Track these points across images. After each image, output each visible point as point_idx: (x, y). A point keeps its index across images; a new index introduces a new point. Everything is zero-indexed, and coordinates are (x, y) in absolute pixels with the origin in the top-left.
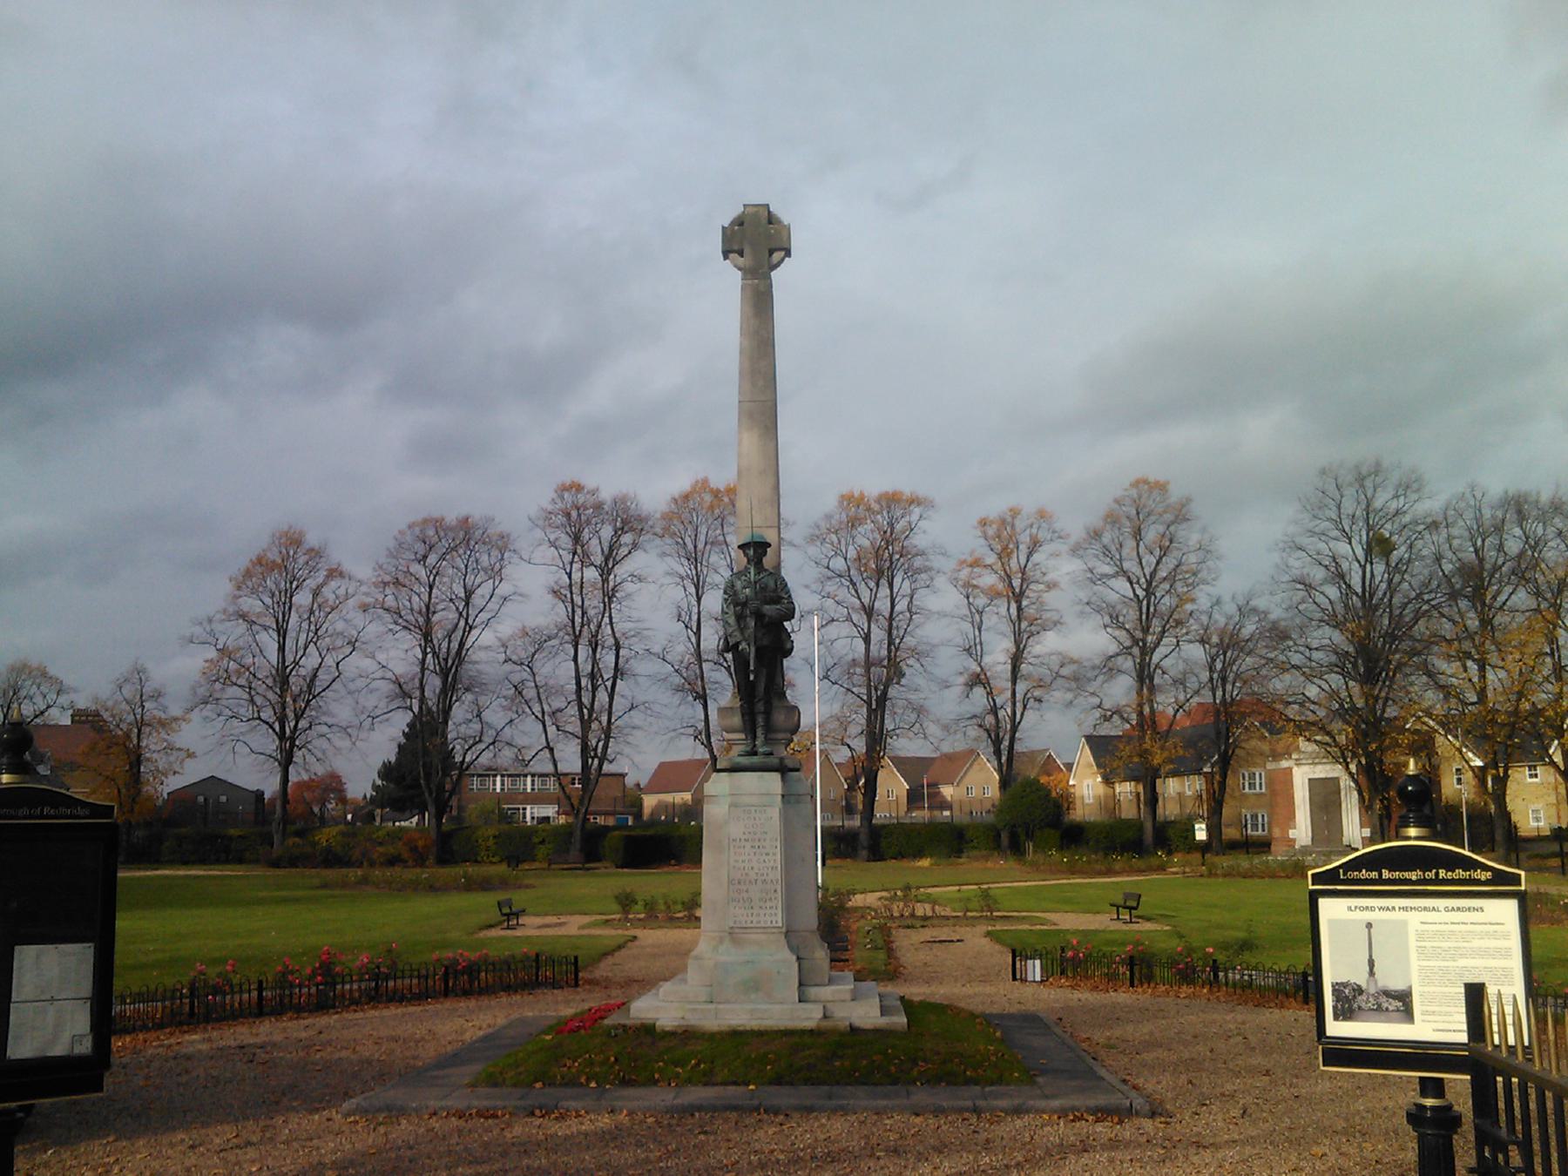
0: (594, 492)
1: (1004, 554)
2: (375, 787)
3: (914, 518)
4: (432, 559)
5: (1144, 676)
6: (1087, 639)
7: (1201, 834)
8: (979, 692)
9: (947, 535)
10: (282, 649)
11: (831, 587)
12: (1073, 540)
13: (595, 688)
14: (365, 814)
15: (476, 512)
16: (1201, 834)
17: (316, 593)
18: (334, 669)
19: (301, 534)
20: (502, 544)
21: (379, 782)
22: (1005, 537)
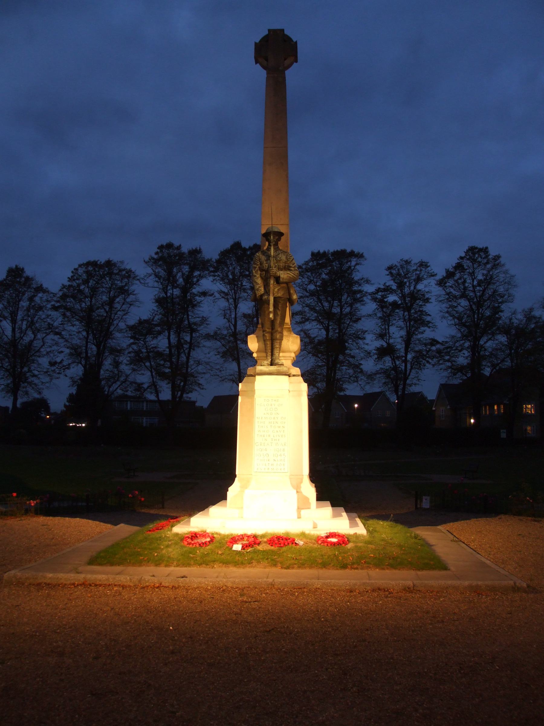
0: (179, 248)
1: (401, 285)
2: (65, 406)
3: (353, 263)
4: (91, 283)
5: (475, 349)
6: (442, 328)
7: (503, 435)
8: (388, 359)
9: (372, 275)
10: (14, 330)
11: (309, 301)
12: (439, 277)
13: (179, 354)
14: (62, 419)
15: (115, 258)
16: (503, 435)
17: (31, 299)
18: (41, 341)
19: (22, 270)
20: (129, 275)
21: (67, 404)
22: (403, 274)
